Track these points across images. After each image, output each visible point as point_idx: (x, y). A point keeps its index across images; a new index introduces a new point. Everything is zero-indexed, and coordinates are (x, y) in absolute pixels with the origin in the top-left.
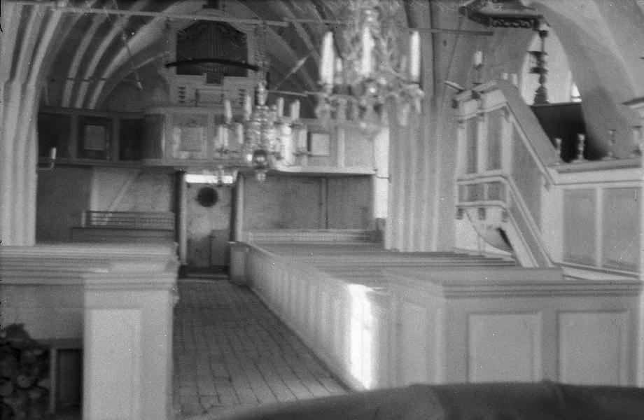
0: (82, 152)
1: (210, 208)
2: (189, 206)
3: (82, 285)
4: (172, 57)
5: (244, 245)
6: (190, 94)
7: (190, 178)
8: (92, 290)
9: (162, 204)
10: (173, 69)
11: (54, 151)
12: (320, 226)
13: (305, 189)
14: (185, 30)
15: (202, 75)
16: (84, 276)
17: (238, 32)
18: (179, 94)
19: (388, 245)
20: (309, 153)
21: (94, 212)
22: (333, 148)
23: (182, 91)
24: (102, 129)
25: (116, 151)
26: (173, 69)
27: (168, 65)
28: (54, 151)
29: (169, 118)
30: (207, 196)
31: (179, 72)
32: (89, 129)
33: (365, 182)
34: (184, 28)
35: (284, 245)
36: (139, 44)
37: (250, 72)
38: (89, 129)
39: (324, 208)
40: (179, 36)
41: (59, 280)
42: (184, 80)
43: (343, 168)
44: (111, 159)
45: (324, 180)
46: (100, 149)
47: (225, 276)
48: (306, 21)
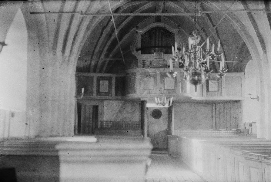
0: (99, 93)
2: (149, 120)
3: (57, 157)
4: (139, 46)
5: (175, 137)
7: (148, 105)
8: (68, 162)
10: (140, 52)
11: (83, 89)
12: (212, 127)
13: (206, 110)
15: (153, 54)
16: (58, 147)
17: (171, 33)
21: (104, 121)
22: (220, 87)
25: (113, 91)
26: (140, 52)
27: (137, 50)
28: (83, 89)
30: (157, 114)
31: (143, 53)
32: (101, 82)
36: (138, 142)
38: (101, 82)
39: (214, 118)
41: (112, 157)
42: (145, 57)
43: (225, 97)
44: (111, 96)
45: (214, 104)
47: (166, 152)
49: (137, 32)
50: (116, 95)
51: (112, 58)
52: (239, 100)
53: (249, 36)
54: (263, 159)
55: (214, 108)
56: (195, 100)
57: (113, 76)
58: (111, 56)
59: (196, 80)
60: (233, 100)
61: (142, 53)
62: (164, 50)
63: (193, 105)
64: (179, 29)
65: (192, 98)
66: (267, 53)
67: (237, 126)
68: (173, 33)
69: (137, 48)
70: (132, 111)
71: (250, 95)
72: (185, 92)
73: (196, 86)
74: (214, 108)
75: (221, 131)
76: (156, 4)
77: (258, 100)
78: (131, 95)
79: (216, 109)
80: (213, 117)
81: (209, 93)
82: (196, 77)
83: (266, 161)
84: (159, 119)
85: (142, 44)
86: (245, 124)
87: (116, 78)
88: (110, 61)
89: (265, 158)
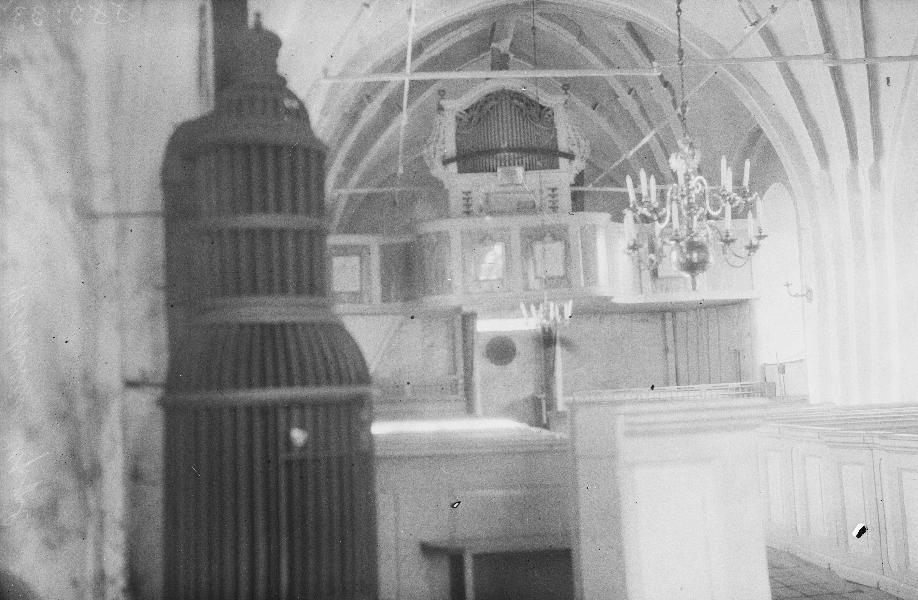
1: (180, 120)
4: (450, 149)
6: (478, 201)
9: (439, 362)
10: (453, 167)
13: (647, 333)
14: (467, 111)
15: (494, 171)
17: (542, 107)
18: (465, 202)
19: (812, 402)
20: (761, 25)
23: (467, 197)
24: (355, 260)
26: (453, 167)
27: (446, 162)
29: (456, 241)
30: (502, 350)
33: (735, 311)
34: (467, 107)
35: (235, 420)
37: (563, 162)
39: (671, 356)
40: (459, 119)
42: (468, 181)
45: (668, 315)
46: (356, 289)
48: (626, 73)
49: (441, 109)
50: (385, 298)
51: (360, 185)
52: (747, 300)
53: (781, 123)
54: (877, 440)
55: (669, 323)
56: (628, 305)
57: (374, 242)
58: (355, 178)
59: (696, 261)
60: (726, 301)
61: (460, 171)
62: (526, 160)
63: (617, 317)
64: (567, 97)
65: (614, 301)
66: (831, 167)
67: (739, 376)
68: (548, 110)
69: (444, 156)
70: (425, 346)
71: (788, 285)
72: (595, 282)
73: (693, 277)
74: (669, 323)
75: (697, 393)
76: (494, 24)
77: (810, 300)
78: (434, 298)
79: (674, 327)
80: (666, 350)
81: (658, 282)
82: (695, 255)
83: (884, 442)
84: (509, 366)
85: (459, 145)
86: (763, 368)
87: (383, 248)
88: (351, 197)
89: (882, 437)
